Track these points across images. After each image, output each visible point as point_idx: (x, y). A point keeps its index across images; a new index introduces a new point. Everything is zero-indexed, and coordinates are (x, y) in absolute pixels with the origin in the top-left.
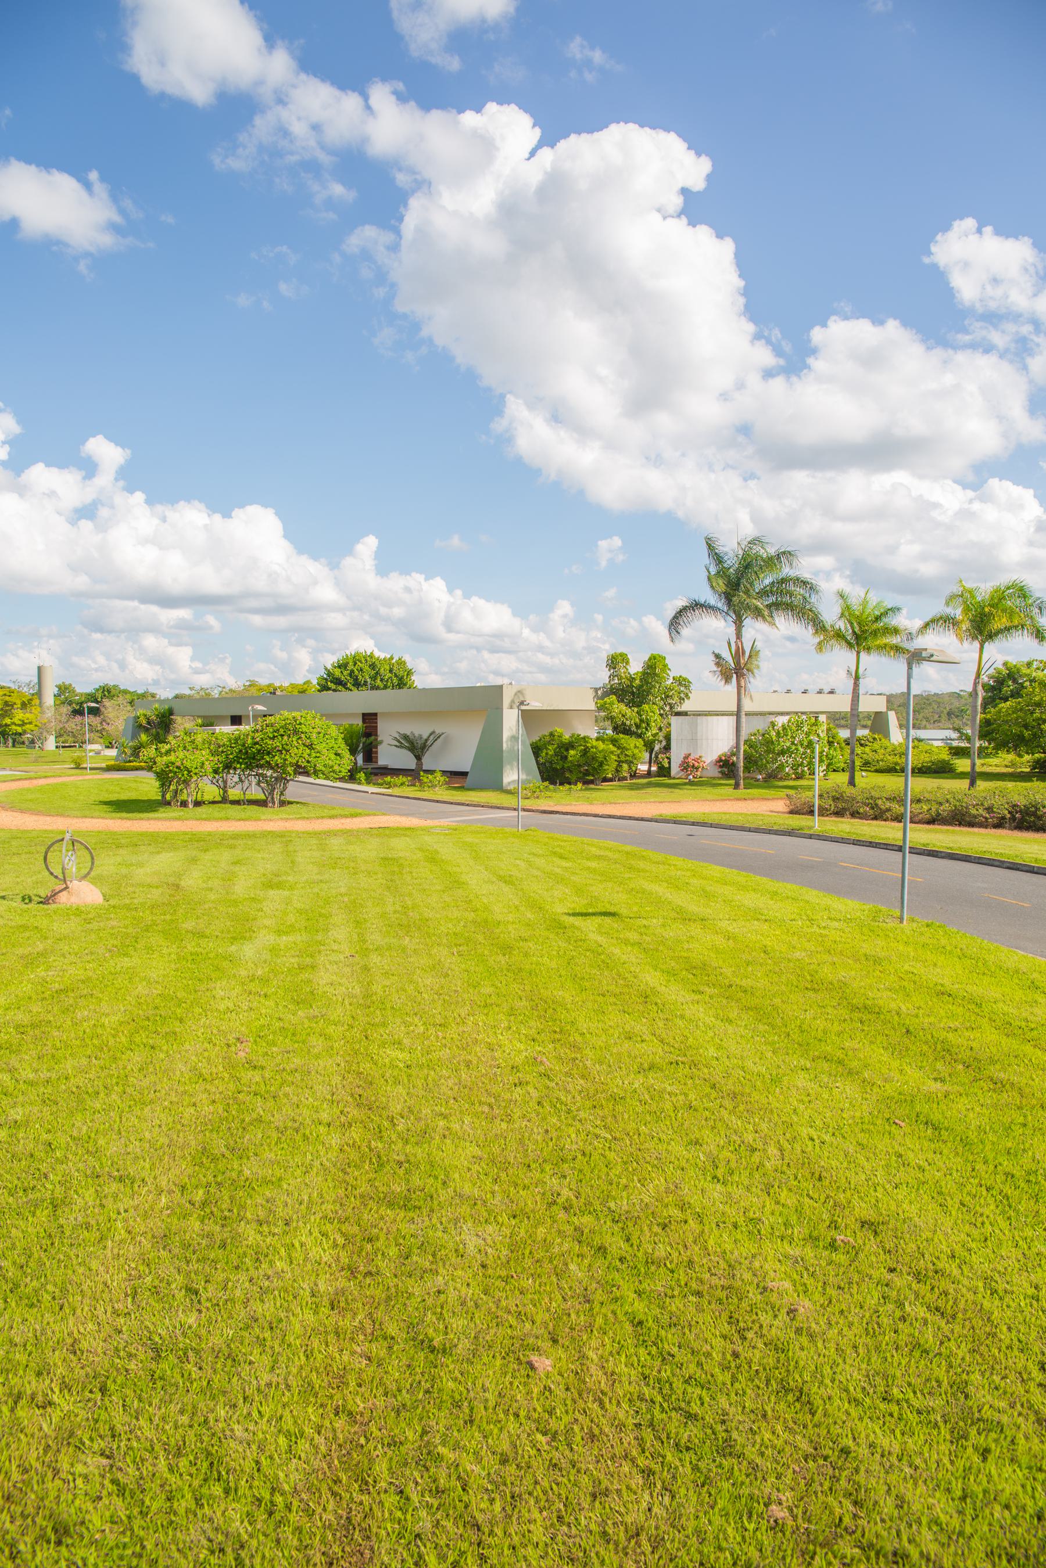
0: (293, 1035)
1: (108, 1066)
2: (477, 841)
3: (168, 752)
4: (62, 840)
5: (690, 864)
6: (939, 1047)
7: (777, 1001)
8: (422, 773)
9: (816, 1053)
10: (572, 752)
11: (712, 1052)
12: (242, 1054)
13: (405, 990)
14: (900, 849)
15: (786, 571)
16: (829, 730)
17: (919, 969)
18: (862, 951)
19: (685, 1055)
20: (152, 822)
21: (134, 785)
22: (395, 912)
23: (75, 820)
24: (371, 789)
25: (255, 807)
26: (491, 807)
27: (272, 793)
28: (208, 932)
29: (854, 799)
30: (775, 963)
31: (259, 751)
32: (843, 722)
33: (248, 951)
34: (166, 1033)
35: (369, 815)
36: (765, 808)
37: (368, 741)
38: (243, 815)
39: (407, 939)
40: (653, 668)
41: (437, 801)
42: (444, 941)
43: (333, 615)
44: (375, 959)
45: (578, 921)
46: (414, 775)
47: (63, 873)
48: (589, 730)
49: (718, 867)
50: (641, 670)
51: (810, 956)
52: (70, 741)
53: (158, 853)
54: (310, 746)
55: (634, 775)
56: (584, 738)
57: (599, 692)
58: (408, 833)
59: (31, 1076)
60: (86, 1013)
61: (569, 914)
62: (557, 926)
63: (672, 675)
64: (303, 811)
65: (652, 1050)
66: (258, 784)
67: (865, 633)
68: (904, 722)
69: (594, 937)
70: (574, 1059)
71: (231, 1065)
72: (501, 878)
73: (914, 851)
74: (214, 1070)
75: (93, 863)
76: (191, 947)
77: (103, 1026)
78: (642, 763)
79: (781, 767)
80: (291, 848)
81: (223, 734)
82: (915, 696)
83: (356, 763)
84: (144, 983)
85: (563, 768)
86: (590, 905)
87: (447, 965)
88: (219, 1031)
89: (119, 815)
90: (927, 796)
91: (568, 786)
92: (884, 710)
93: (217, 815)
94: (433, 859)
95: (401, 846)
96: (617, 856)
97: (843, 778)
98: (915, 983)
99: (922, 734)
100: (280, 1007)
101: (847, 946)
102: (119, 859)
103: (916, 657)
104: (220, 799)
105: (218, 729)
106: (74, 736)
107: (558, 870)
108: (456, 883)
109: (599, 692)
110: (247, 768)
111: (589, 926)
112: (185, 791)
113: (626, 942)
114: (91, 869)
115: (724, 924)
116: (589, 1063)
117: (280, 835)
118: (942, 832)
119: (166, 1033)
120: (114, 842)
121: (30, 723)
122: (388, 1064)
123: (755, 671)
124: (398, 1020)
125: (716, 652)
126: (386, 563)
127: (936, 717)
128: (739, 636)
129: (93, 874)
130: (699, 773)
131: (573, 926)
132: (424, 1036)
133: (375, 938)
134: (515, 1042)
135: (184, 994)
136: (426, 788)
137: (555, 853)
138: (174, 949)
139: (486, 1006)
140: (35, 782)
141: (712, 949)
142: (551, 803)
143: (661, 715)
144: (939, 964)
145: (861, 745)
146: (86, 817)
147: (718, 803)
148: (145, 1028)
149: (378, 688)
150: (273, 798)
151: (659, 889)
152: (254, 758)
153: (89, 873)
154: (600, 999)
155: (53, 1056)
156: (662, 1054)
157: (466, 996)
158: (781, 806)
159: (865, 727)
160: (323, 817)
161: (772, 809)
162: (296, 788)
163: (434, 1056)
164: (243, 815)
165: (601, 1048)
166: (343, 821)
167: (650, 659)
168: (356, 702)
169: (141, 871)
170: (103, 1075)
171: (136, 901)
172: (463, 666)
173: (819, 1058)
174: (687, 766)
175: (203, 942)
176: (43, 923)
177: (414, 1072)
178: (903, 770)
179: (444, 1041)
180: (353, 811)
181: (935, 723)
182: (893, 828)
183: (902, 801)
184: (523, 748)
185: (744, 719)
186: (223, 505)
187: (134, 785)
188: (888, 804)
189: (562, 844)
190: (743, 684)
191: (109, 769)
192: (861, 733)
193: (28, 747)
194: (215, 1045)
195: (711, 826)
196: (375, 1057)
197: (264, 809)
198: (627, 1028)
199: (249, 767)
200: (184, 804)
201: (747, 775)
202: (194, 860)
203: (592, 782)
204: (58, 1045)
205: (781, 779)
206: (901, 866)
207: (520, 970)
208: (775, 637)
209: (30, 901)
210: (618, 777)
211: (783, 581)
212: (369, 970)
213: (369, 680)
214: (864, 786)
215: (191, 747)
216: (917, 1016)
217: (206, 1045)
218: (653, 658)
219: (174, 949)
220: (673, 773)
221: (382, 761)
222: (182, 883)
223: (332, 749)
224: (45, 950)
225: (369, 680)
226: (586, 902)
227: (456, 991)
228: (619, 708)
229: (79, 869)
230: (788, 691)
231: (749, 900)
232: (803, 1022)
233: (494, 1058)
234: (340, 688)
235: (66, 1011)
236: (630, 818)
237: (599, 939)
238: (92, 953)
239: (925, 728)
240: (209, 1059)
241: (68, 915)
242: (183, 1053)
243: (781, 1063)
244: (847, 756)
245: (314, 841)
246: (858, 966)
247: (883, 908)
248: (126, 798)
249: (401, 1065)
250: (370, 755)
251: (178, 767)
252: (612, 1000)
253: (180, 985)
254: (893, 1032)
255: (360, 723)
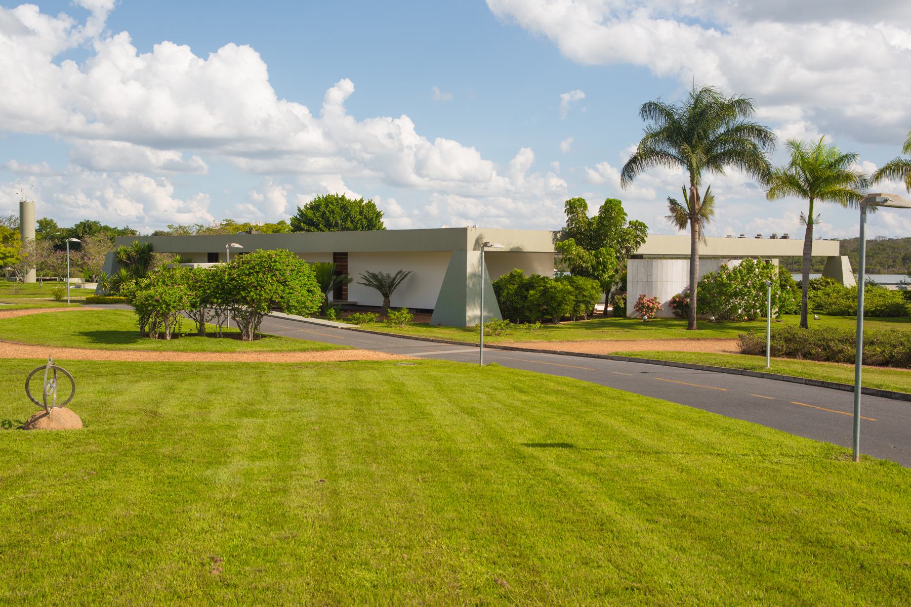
0: (265, 555)
1: (85, 584)
2: (441, 375)
3: (148, 287)
4: (45, 367)
5: (645, 400)
6: (895, 583)
7: (730, 532)
8: (389, 311)
9: (769, 584)
10: (532, 292)
11: (666, 579)
12: (215, 573)
13: (372, 514)
14: (853, 389)
15: (740, 119)
16: (781, 273)
17: (872, 506)
18: (814, 487)
19: (640, 582)
20: (130, 353)
21: (113, 317)
22: (363, 440)
23: (55, 350)
24: (341, 324)
25: (231, 340)
26: (455, 343)
27: (246, 327)
28: (184, 457)
29: (806, 340)
30: (727, 496)
31: (235, 286)
32: (796, 267)
33: (223, 475)
34: (143, 553)
35: (338, 349)
36: (718, 348)
37: (338, 280)
38: (218, 347)
39: (375, 466)
40: (611, 209)
41: (404, 337)
42: (410, 468)
43: (312, 160)
44: (344, 484)
45: (536, 452)
46: (382, 312)
47: (44, 399)
48: (547, 271)
49: (672, 403)
50: (597, 215)
51: (763, 490)
52: (51, 274)
53: (137, 382)
54: (284, 283)
55: (591, 314)
56: (543, 279)
57: (559, 235)
58: (376, 366)
59: (8, 594)
60: (64, 533)
61: (528, 445)
62: (516, 455)
63: (628, 219)
64: (276, 344)
65: (608, 575)
66: (234, 318)
67: (819, 178)
68: (857, 267)
69: (552, 466)
70: (533, 582)
71: (205, 583)
72: (464, 410)
73: (866, 391)
74: (189, 588)
75: (74, 390)
76: (167, 471)
77: (80, 545)
78: (599, 303)
79: (735, 308)
80: (264, 379)
81: (200, 269)
82: (868, 242)
83: (326, 300)
84: (122, 505)
85: (523, 307)
86: (548, 436)
87: (412, 491)
88: (194, 551)
89: (98, 345)
90: (880, 338)
91: (527, 325)
92: (837, 254)
93: (193, 346)
94: (399, 390)
95: (368, 378)
96: (574, 391)
97: (796, 320)
98: (869, 519)
99: (877, 278)
100: (253, 528)
101: (800, 481)
102: (98, 387)
103: (871, 203)
104: (197, 332)
105: (196, 265)
106: (55, 270)
107: (518, 404)
108: (421, 414)
109: (559, 235)
110: (223, 303)
111: (548, 456)
112: (163, 324)
113: (583, 472)
114: (72, 396)
115: (677, 458)
116: (547, 586)
117: (254, 367)
118: (896, 374)
119: (143, 553)
120: (93, 371)
121: (12, 257)
122: (355, 583)
123: (710, 216)
124: (366, 542)
125: (672, 197)
126: (357, 108)
127: (891, 262)
128: (694, 182)
129: (73, 400)
130: (653, 314)
131: (532, 456)
132: (390, 558)
133: (344, 464)
134: (477, 565)
135: (160, 515)
136: (393, 325)
137: (515, 387)
138: (151, 472)
139: (449, 530)
140: (16, 313)
141: (666, 481)
142: (512, 340)
143: (617, 257)
144: (894, 502)
145: (814, 289)
146: (66, 347)
147: (671, 342)
148: (122, 548)
149: (348, 229)
150: (247, 332)
151: (615, 423)
152: (230, 293)
153: (69, 400)
154: (558, 525)
155: (31, 575)
156: (617, 579)
157: (430, 520)
158: (733, 346)
159: (817, 271)
160: (294, 351)
161: (725, 349)
162: (271, 321)
163: (400, 576)
164: (218, 347)
165: (559, 572)
166: (314, 354)
167: (606, 203)
168: (330, 241)
169: (120, 399)
170: (80, 593)
171: (115, 427)
172: (433, 209)
173: (772, 588)
174: (641, 307)
175: (180, 467)
176: (23, 447)
177: (380, 591)
178: (856, 313)
179: (409, 562)
180: (323, 344)
181: (890, 269)
182: (846, 369)
183: (854, 343)
184: (485, 285)
185: (697, 262)
186: (203, 49)
187: (113, 317)
188: (840, 346)
189: (522, 379)
190: (697, 228)
191: (89, 302)
192: (813, 277)
193: (9, 280)
194: (190, 564)
195: (665, 364)
196: (343, 577)
197: (239, 342)
198: (584, 554)
199: (226, 302)
200: (162, 336)
201: (700, 316)
202: (171, 389)
203: (550, 321)
204: (36, 564)
205: (733, 320)
206: (853, 406)
207: (482, 497)
208: (728, 182)
209: (10, 426)
210: (575, 317)
211: (739, 129)
212: (338, 494)
213: (340, 222)
214: (816, 328)
215: (168, 282)
216: (871, 552)
217: (181, 564)
218: (609, 203)
219: (151, 472)
220: (628, 313)
221: (352, 298)
222: (160, 411)
223: (304, 285)
224: (25, 473)
225: (340, 222)
226: (544, 434)
227: (420, 516)
228: (577, 251)
229: (59, 396)
230: (742, 236)
231: (702, 434)
232: (755, 554)
233: (456, 580)
234: (312, 228)
235: (44, 531)
236: (587, 355)
237: (557, 468)
238: (71, 476)
239: (879, 273)
240: (184, 578)
241: (47, 439)
242: (159, 572)
243: (734, 592)
244: (800, 299)
245: (286, 373)
246: (810, 501)
247: (835, 446)
248: (105, 329)
249: (368, 585)
250: (340, 292)
251: (157, 301)
252: (570, 526)
253: (156, 506)
254: (846, 567)
255: (331, 262)
